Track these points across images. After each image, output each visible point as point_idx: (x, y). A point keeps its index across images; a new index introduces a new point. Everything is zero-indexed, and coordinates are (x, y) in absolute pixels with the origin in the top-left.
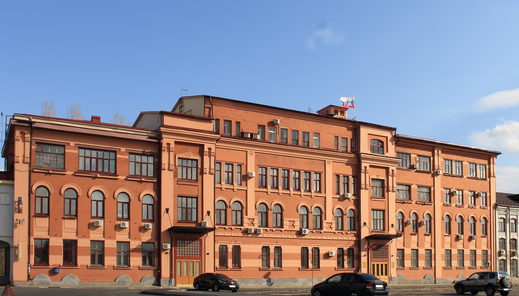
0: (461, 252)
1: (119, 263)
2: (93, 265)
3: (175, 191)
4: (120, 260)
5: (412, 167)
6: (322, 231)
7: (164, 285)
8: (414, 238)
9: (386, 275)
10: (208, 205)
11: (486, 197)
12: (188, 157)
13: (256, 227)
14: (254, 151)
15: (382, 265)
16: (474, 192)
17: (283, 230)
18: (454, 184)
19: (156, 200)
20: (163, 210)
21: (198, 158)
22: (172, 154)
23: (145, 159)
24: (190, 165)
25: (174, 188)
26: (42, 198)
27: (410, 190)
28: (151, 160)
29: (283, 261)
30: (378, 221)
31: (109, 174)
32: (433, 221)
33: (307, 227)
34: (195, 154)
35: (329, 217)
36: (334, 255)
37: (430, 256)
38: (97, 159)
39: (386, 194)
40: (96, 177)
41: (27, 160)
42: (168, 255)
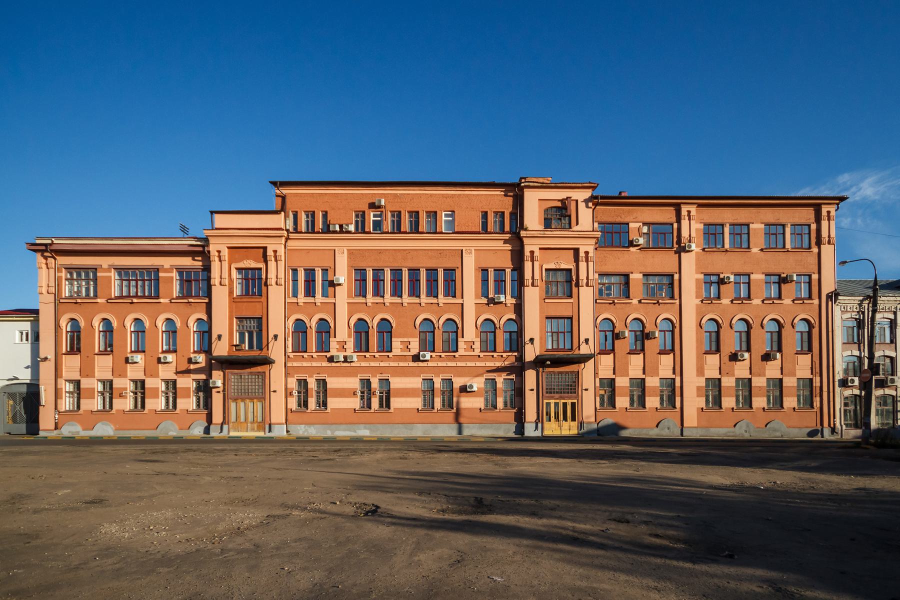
0: (640, 385)
1: (632, 404)
5: (631, 244)
7: (214, 433)
8: (636, 361)
9: (573, 419)
11: (810, 283)
12: (248, 266)
14: (473, 249)
16: (780, 275)
17: (391, 355)
18: (727, 264)
22: (536, 264)
27: (627, 283)
31: (150, 297)
32: (677, 331)
34: (256, 261)
35: (470, 333)
39: (575, 290)
40: (132, 303)
41: (52, 290)
42: (221, 395)
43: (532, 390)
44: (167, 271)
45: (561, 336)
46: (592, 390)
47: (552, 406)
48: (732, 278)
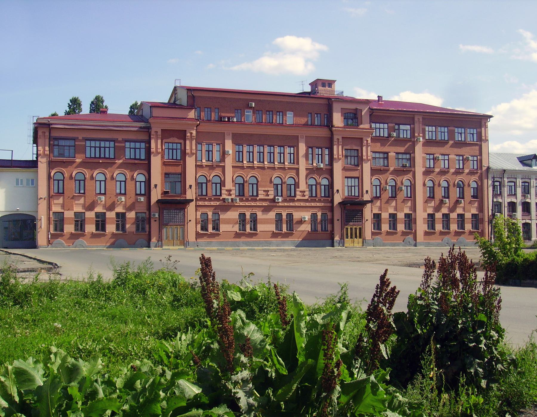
0: (393, 216)
2: (97, 232)
3: (162, 170)
4: (139, 227)
6: (296, 199)
9: (360, 237)
10: (190, 180)
13: (233, 197)
15: (356, 228)
19: (147, 178)
20: (152, 186)
21: (359, 148)
23: (138, 145)
24: (175, 147)
25: (161, 167)
26: (216, 184)
28: (143, 145)
29: (258, 225)
30: (353, 188)
33: (282, 196)
36: (307, 219)
37: (410, 220)
38: (100, 147)
43: (338, 220)
44: (80, 141)
45: (353, 188)
46: (193, 221)
47: (349, 230)
48: (470, 158)
